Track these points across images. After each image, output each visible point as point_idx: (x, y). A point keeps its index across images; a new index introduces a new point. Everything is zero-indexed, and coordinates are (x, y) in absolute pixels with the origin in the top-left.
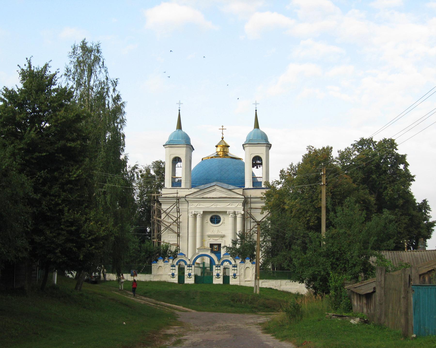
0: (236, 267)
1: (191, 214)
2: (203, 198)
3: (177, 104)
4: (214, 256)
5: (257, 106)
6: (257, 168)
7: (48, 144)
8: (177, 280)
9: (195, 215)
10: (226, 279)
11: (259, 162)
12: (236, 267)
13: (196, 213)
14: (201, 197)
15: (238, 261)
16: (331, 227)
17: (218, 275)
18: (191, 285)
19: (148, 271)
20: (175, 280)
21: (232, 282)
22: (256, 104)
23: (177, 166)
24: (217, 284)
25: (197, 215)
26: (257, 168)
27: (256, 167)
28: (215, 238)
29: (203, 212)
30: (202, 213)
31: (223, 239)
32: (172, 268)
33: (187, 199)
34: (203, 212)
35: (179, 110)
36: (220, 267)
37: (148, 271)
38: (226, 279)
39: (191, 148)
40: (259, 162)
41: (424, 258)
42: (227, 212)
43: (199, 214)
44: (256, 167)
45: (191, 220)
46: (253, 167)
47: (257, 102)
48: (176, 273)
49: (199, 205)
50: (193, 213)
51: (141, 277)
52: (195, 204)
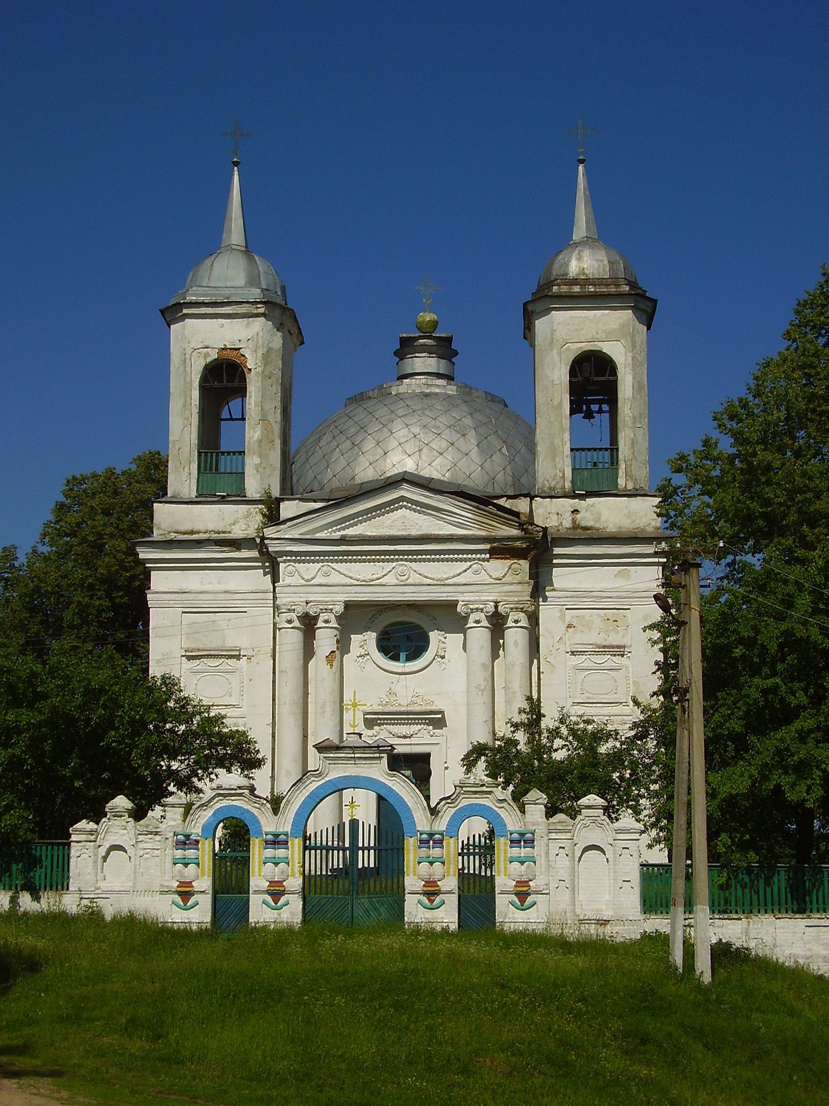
0: (530, 843)
2: (343, 540)
7: (670, 689)
9: (309, 624)
10: (477, 896)
12: (530, 843)
14: (338, 535)
15: (536, 812)
17: (431, 892)
18: (284, 934)
20: (199, 914)
21: (509, 916)
23: (225, 414)
25: (316, 618)
29: (348, 605)
30: (339, 609)
32: (179, 853)
34: (348, 605)
38: (477, 896)
39: (535, 648)
43: (323, 617)
45: (292, 639)
48: (204, 883)
49: (327, 575)
50: (300, 610)
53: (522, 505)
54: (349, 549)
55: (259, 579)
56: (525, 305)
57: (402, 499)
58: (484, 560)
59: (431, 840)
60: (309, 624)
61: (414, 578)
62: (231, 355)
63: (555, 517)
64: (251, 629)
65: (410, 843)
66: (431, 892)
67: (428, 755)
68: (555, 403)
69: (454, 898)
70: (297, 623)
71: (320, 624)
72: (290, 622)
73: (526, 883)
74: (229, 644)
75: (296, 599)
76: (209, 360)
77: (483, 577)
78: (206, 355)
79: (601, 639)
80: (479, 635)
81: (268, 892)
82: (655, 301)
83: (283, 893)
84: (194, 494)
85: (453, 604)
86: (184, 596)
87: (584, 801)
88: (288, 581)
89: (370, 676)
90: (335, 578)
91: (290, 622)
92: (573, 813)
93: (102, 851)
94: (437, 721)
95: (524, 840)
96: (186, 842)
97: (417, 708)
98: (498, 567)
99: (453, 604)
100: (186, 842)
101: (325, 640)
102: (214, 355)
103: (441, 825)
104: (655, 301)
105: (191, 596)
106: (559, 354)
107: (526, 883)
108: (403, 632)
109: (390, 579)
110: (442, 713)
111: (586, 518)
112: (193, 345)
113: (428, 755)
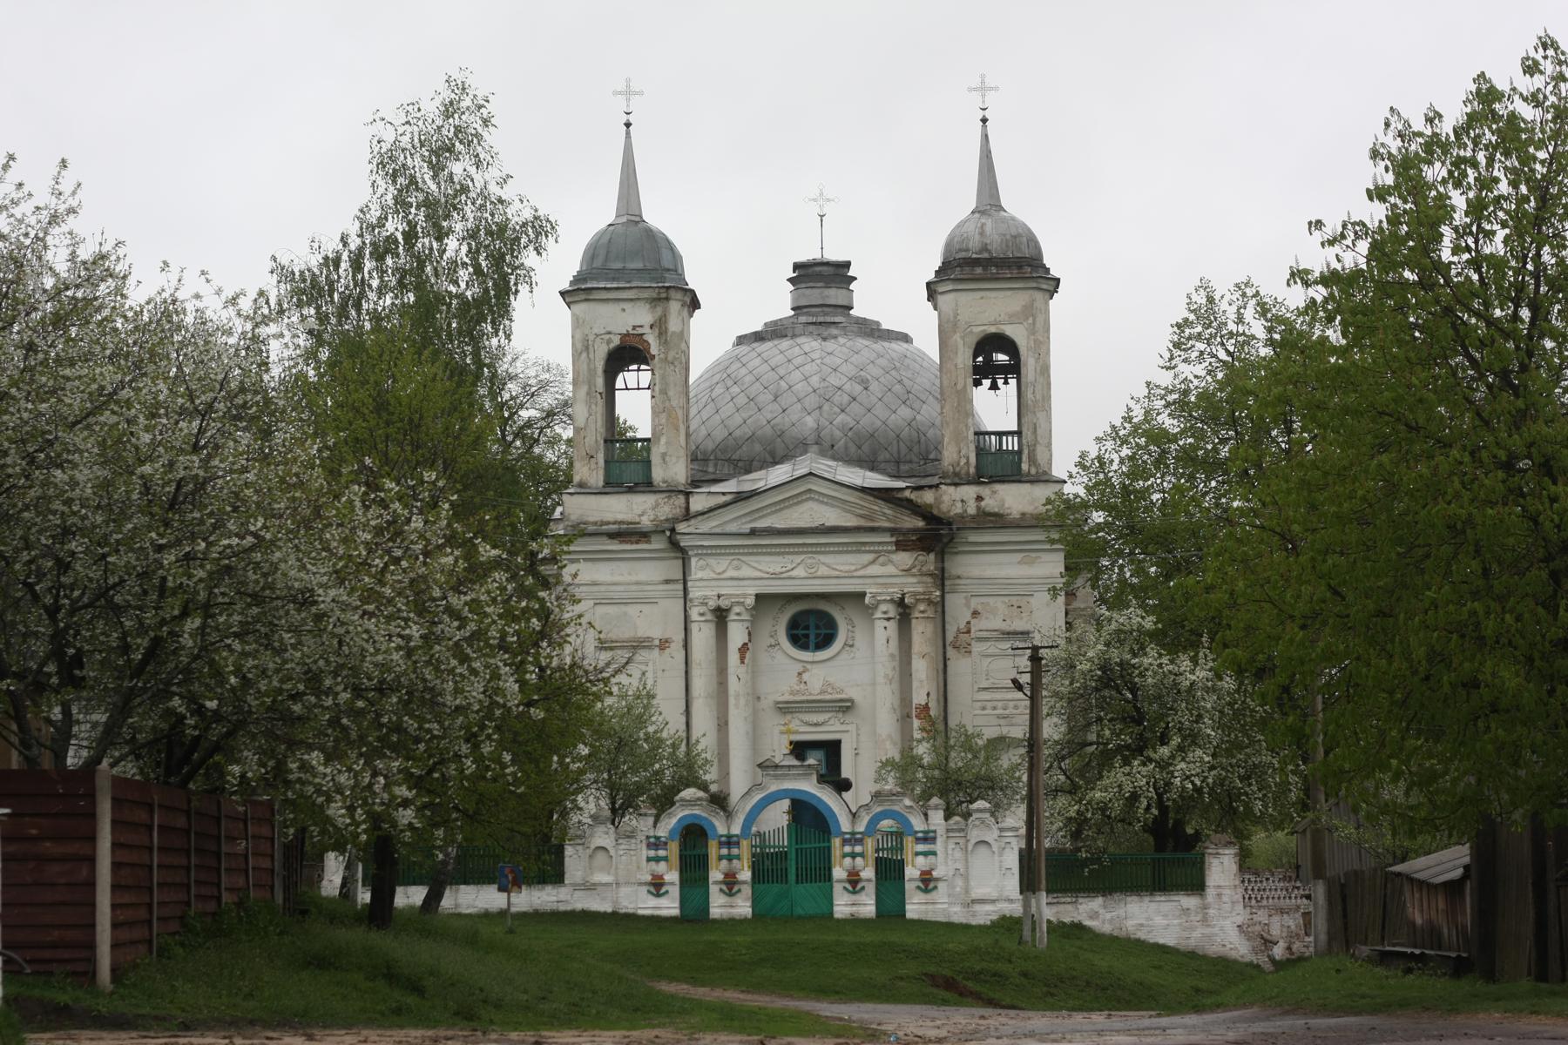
0: (933, 840)
1: (703, 609)
3: (616, 93)
4: (826, 796)
5: (990, 96)
6: (994, 387)
8: (677, 904)
9: (721, 616)
11: (1001, 358)
13: (724, 603)
14: (746, 528)
15: (937, 818)
16: (1389, 179)
17: (854, 881)
19: (554, 874)
21: (916, 907)
22: (628, 93)
23: (619, 383)
24: (919, 922)
25: (728, 610)
26: (994, 387)
27: (987, 383)
28: (814, 718)
29: (758, 596)
30: (750, 601)
31: (848, 718)
32: (652, 853)
33: (684, 542)
34: (758, 596)
35: (984, 120)
36: (860, 842)
37: (554, 874)
40: (1001, 358)
41: (1417, 895)
42: (863, 594)
43: (737, 609)
44: (987, 383)
45: (702, 636)
46: (977, 383)
47: (635, 87)
48: (672, 877)
49: (738, 568)
50: (712, 604)
51: (529, 899)
52: (721, 564)
53: (928, 497)
54: (761, 537)
55: (673, 569)
56: (928, 284)
57: (810, 491)
58: (890, 552)
59: (853, 839)
60: (721, 616)
61: (823, 571)
62: (635, 343)
63: (959, 505)
64: (657, 619)
65: (836, 842)
66: (854, 881)
67: (839, 742)
68: (959, 387)
69: (677, 889)
70: (709, 617)
71: (732, 617)
72: (702, 615)
73: (929, 872)
74: (641, 633)
75: (708, 593)
76: (612, 346)
77: (891, 569)
78: (609, 342)
79: (1005, 627)
80: (884, 632)
81: (650, 884)
82: (1058, 280)
83: (662, 885)
84: (601, 483)
85: (863, 595)
86: (596, 588)
87: (975, 806)
88: (700, 575)
89: (787, 670)
90: (746, 572)
91: (702, 615)
92: (967, 815)
93: (589, 852)
94: (845, 707)
95: (928, 838)
96: (655, 844)
97: (828, 697)
98: (906, 559)
99: (863, 595)
100: (655, 844)
101: (737, 634)
102: (616, 341)
103: (861, 828)
104: (1058, 280)
105: (603, 588)
106: (963, 338)
107: (929, 872)
108: (812, 625)
109: (800, 572)
110: (851, 701)
111: (990, 504)
112: (596, 331)
113: (839, 742)
